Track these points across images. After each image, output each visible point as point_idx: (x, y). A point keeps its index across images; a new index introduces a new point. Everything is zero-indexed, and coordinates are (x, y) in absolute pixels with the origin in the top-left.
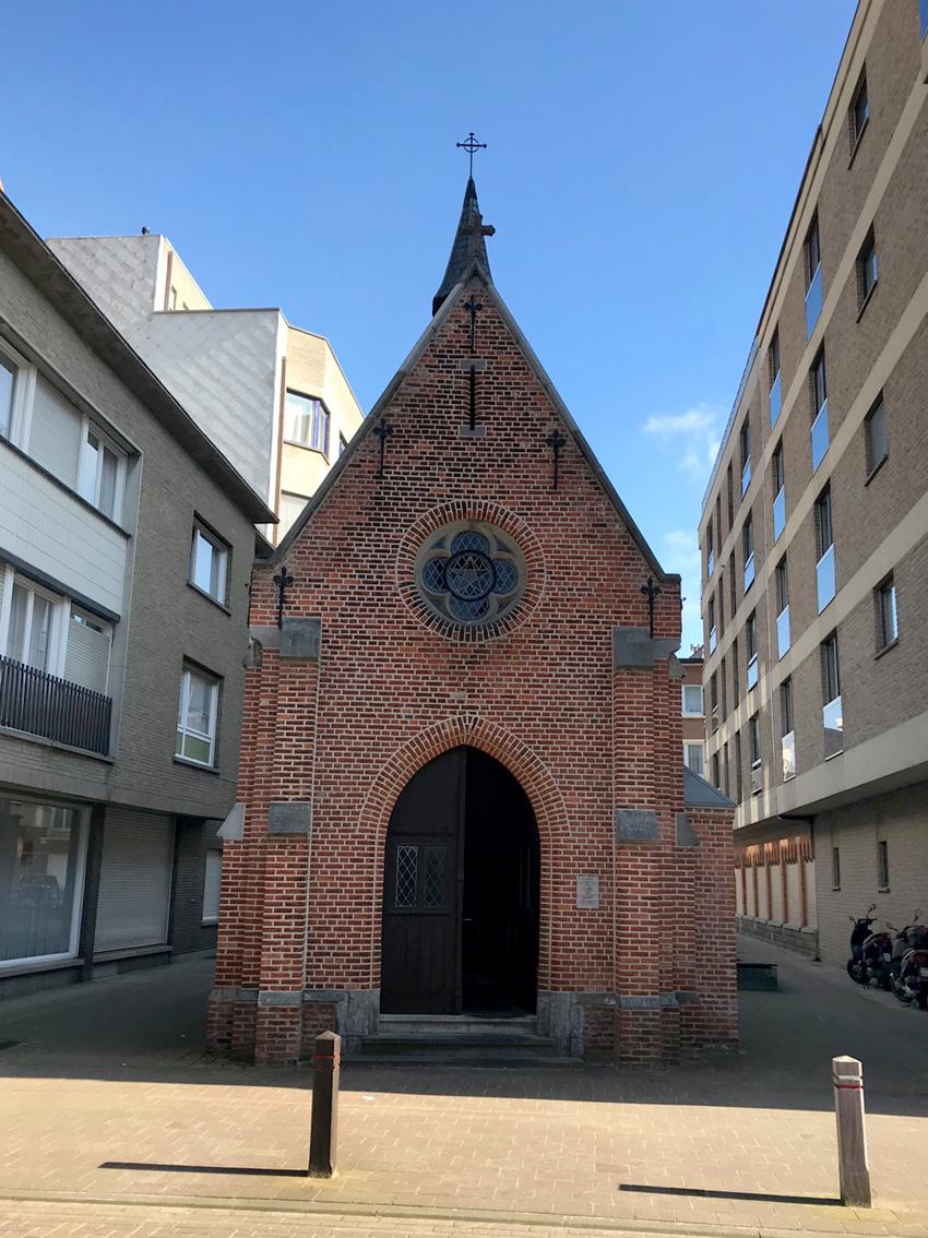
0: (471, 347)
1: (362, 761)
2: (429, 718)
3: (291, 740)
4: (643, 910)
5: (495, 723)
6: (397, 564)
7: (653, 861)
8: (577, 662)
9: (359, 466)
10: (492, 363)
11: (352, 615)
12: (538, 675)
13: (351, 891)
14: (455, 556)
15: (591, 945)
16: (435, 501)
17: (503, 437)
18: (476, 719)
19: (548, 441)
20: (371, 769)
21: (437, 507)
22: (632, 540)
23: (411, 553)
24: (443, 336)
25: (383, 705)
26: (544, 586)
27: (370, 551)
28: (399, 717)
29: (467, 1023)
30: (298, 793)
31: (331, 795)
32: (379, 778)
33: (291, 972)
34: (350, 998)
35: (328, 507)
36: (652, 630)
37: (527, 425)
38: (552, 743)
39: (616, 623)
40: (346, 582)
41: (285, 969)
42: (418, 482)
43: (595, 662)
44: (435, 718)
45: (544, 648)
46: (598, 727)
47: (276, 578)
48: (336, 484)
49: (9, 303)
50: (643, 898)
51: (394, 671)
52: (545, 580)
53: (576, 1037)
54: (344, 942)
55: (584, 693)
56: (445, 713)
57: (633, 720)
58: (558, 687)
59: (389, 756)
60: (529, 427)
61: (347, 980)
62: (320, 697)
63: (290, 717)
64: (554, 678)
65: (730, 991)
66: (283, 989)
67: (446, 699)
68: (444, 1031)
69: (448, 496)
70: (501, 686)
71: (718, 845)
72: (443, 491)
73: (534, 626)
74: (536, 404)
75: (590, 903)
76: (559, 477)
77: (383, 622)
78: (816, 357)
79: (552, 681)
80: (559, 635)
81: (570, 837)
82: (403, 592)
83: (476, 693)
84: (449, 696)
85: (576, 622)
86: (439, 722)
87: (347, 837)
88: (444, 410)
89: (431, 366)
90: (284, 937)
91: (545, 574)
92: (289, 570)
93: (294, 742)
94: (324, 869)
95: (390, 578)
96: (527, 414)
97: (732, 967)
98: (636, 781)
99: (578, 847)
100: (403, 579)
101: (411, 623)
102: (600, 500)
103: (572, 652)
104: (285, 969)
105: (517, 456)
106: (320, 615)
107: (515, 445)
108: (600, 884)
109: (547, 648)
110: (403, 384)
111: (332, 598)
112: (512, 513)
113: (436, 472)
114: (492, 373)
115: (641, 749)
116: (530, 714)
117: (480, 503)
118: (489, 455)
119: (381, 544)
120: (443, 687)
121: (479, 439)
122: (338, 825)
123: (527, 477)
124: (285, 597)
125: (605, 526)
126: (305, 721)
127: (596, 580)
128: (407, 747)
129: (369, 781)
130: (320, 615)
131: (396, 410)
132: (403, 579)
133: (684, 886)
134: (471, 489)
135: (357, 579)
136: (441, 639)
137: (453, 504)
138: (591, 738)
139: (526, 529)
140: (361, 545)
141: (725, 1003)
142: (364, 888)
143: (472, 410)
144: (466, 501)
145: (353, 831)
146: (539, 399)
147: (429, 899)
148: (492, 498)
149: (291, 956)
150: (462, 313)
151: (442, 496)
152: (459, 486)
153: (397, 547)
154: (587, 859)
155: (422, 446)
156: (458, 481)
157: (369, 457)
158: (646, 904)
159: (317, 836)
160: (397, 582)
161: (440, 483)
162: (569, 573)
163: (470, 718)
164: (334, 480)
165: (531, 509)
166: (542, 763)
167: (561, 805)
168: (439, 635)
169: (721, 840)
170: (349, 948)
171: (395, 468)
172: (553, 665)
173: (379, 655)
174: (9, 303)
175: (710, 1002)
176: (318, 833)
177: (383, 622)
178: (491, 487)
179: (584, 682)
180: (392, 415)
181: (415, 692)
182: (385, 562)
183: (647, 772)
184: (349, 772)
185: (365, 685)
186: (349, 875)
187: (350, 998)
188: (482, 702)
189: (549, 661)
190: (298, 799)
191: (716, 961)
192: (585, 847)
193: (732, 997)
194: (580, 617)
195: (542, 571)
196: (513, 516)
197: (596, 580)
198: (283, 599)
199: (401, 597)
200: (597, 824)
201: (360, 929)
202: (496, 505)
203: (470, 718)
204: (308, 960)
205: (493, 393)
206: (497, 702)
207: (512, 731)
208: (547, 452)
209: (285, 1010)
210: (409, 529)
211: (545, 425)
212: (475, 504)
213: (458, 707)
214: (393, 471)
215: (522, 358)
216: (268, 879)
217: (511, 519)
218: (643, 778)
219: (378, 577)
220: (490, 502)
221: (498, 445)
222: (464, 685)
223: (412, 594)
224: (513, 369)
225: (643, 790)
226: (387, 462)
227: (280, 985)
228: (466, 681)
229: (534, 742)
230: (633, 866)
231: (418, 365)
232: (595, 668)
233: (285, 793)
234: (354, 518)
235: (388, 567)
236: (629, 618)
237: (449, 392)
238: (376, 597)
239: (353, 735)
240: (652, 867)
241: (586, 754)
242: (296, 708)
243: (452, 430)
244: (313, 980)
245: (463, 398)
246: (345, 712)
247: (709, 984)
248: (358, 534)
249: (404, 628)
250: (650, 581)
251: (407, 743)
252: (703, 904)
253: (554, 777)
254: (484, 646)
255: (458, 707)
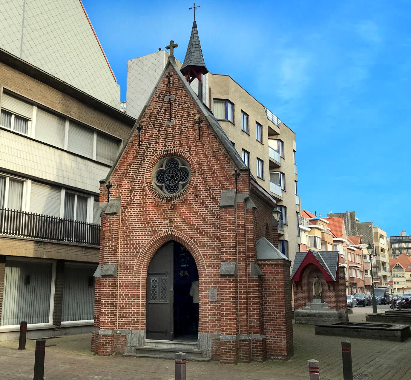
0: (169, 92)
1: (135, 248)
2: (156, 231)
3: (110, 242)
4: (229, 301)
5: (179, 232)
6: (145, 176)
7: (233, 282)
8: (208, 206)
9: (132, 142)
10: (176, 96)
11: (131, 196)
12: (194, 212)
13: (132, 295)
14: (167, 170)
15: (215, 315)
16: (157, 151)
17: (181, 123)
18: (172, 230)
19: (197, 122)
20: (138, 251)
21: (158, 153)
22: (229, 156)
23: (150, 171)
24: (159, 89)
25: (141, 227)
26: (196, 177)
27: (136, 172)
28: (146, 231)
29: (174, 344)
30: (112, 261)
31: (125, 261)
32: (140, 254)
33: (109, 323)
34: (132, 333)
35: (123, 158)
36: (236, 191)
37: (189, 117)
38: (199, 238)
39: (223, 189)
40: (129, 184)
41: (108, 322)
42: (152, 145)
43: (215, 205)
44: (159, 231)
45: (196, 201)
46: (216, 230)
47: (107, 186)
48: (125, 150)
49: (51, 101)
50: (229, 297)
51: (144, 215)
52: (196, 175)
53: (208, 350)
54: (130, 313)
55: (211, 217)
56: (162, 229)
57: (227, 227)
58: (201, 216)
59: (143, 246)
60: (190, 118)
61: (131, 327)
62: (121, 226)
63: (109, 234)
64: (200, 213)
65: (283, 335)
66: (107, 329)
67: (162, 224)
68: (167, 346)
69: (161, 148)
70: (181, 217)
71: (277, 275)
72: (160, 147)
73: (193, 193)
74: (192, 108)
75: (214, 299)
76: (201, 135)
77: (141, 197)
78: (50, 113)
79: (199, 214)
80: (202, 196)
81: (207, 274)
82: (147, 185)
83: (172, 221)
84: (163, 222)
85: (208, 190)
86: (160, 232)
87: (130, 276)
88: (160, 117)
89: (155, 102)
90: (107, 311)
91: (196, 173)
92: (111, 182)
93: (111, 243)
94: (123, 287)
95: (143, 181)
96: (189, 113)
97: (284, 326)
98: (228, 251)
99: (210, 277)
100: (147, 181)
101: (150, 197)
102: (216, 141)
103: (207, 202)
104: (108, 322)
105: (186, 129)
106: (121, 197)
107: (185, 125)
108: (217, 291)
109: (197, 201)
110: (146, 110)
111: (124, 191)
112: (184, 151)
113: (158, 140)
114: (176, 100)
115: (230, 238)
116: (191, 227)
117: (173, 149)
118: (176, 131)
119: (140, 169)
120: (161, 219)
121: (172, 125)
122: (127, 271)
123: (189, 137)
124: (110, 192)
125: (218, 151)
126: (114, 235)
127: (215, 173)
128: (149, 242)
129: (137, 255)
130: (121, 197)
131: (144, 120)
132: (147, 181)
133: (254, 292)
134: (169, 144)
135: (132, 183)
136: (160, 202)
137: (163, 151)
138: (214, 235)
139: (189, 156)
140: (133, 170)
141: (281, 340)
142: (136, 294)
143: (171, 114)
144: (168, 149)
145: (132, 273)
146: (193, 106)
147: (162, 297)
148: (177, 147)
149: (109, 317)
150: (166, 80)
151: (160, 149)
152: (165, 144)
153: (145, 169)
154: (213, 282)
155: (153, 131)
156: (165, 142)
157: (136, 138)
158: (230, 299)
159: (121, 275)
160: (145, 182)
161: (159, 144)
162: (205, 172)
163: (170, 230)
164: (124, 148)
165: (191, 149)
166: (196, 245)
167: (203, 261)
168: (159, 200)
169: (278, 273)
170: (131, 315)
171: (144, 141)
172: (199, 208)
173: (139, 209)
174: (51, 101)
175: (275, 340)
176: (121, 274)
177: (141, 197)
178: (177, 143)
179: (211, 213)
180: (143, 122)
181: (151, 222)
182: (141, 175)
183: (232, 247)
184: (131, 252)
185: (135, 221)
186: (131, 289)
187: (132, 333)
188: (175, 224)
189: (198, 206)
190: (112, 263)
191: (277, 323)
192: (212, 277)
193: (283, 338)
194: (210, 188)
195: (195, 172)
196: (184, 152)
197: (215, 173)
198: (109, 193)
199: (146, 188)
200: (216, 268)
201: (135, 308)
202: (178, 149)
203: (170, 230)
204: (119, 319)
205: (177, 107)
206: (179, 224)
207: (185, 234)
208: (196, 126)
209: (107, 336)
210: (149, 162)
211: (195, 116)
212: (171, 150)
213: (166, 226)
214: (143, 142)
215: (187, 92)
216: (102, 291)
217: (184, 154)
218: (231, 249)
219: (139, 181)
220: (176, 148)
221: (179, 126)
222: (168, 218)
223: (150, 186)
224: (184, 97)
225: (231, 254)
226: (142, 139)
227: (106, 327)
228: (169, 216)
229: (193, 238)
230: (225, 284)
231: (151, 102)
232: (215, 208)
233: (108, 261)
234: (131, 161)
235: (142, 177)
236: (228, 187)
237: (162, 110)
238: (138, 189)
239: (132, 239)
240: (232, 285)
241: (212, 241)
242: (111, 231)
243: (163, 124)
244: (120, 326)
245: (167, 111)
246: (129, 231)
247: (274, 332)
248: (132, 167)
249: (147, 199)
250: (236, 171)
251: (149, 241)
252: (271, 300)
253: (200, 251)
254: (174, 203)
255: (166, 226)
